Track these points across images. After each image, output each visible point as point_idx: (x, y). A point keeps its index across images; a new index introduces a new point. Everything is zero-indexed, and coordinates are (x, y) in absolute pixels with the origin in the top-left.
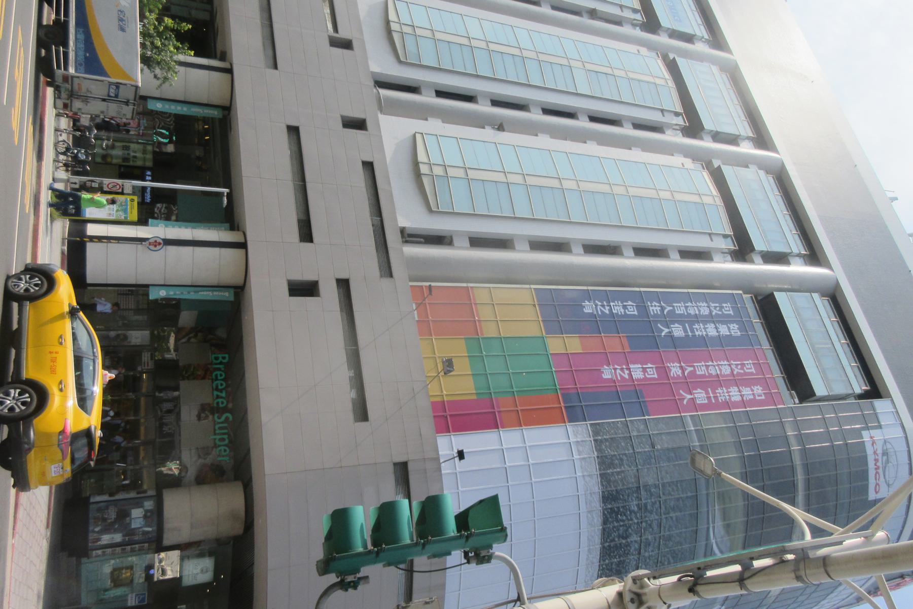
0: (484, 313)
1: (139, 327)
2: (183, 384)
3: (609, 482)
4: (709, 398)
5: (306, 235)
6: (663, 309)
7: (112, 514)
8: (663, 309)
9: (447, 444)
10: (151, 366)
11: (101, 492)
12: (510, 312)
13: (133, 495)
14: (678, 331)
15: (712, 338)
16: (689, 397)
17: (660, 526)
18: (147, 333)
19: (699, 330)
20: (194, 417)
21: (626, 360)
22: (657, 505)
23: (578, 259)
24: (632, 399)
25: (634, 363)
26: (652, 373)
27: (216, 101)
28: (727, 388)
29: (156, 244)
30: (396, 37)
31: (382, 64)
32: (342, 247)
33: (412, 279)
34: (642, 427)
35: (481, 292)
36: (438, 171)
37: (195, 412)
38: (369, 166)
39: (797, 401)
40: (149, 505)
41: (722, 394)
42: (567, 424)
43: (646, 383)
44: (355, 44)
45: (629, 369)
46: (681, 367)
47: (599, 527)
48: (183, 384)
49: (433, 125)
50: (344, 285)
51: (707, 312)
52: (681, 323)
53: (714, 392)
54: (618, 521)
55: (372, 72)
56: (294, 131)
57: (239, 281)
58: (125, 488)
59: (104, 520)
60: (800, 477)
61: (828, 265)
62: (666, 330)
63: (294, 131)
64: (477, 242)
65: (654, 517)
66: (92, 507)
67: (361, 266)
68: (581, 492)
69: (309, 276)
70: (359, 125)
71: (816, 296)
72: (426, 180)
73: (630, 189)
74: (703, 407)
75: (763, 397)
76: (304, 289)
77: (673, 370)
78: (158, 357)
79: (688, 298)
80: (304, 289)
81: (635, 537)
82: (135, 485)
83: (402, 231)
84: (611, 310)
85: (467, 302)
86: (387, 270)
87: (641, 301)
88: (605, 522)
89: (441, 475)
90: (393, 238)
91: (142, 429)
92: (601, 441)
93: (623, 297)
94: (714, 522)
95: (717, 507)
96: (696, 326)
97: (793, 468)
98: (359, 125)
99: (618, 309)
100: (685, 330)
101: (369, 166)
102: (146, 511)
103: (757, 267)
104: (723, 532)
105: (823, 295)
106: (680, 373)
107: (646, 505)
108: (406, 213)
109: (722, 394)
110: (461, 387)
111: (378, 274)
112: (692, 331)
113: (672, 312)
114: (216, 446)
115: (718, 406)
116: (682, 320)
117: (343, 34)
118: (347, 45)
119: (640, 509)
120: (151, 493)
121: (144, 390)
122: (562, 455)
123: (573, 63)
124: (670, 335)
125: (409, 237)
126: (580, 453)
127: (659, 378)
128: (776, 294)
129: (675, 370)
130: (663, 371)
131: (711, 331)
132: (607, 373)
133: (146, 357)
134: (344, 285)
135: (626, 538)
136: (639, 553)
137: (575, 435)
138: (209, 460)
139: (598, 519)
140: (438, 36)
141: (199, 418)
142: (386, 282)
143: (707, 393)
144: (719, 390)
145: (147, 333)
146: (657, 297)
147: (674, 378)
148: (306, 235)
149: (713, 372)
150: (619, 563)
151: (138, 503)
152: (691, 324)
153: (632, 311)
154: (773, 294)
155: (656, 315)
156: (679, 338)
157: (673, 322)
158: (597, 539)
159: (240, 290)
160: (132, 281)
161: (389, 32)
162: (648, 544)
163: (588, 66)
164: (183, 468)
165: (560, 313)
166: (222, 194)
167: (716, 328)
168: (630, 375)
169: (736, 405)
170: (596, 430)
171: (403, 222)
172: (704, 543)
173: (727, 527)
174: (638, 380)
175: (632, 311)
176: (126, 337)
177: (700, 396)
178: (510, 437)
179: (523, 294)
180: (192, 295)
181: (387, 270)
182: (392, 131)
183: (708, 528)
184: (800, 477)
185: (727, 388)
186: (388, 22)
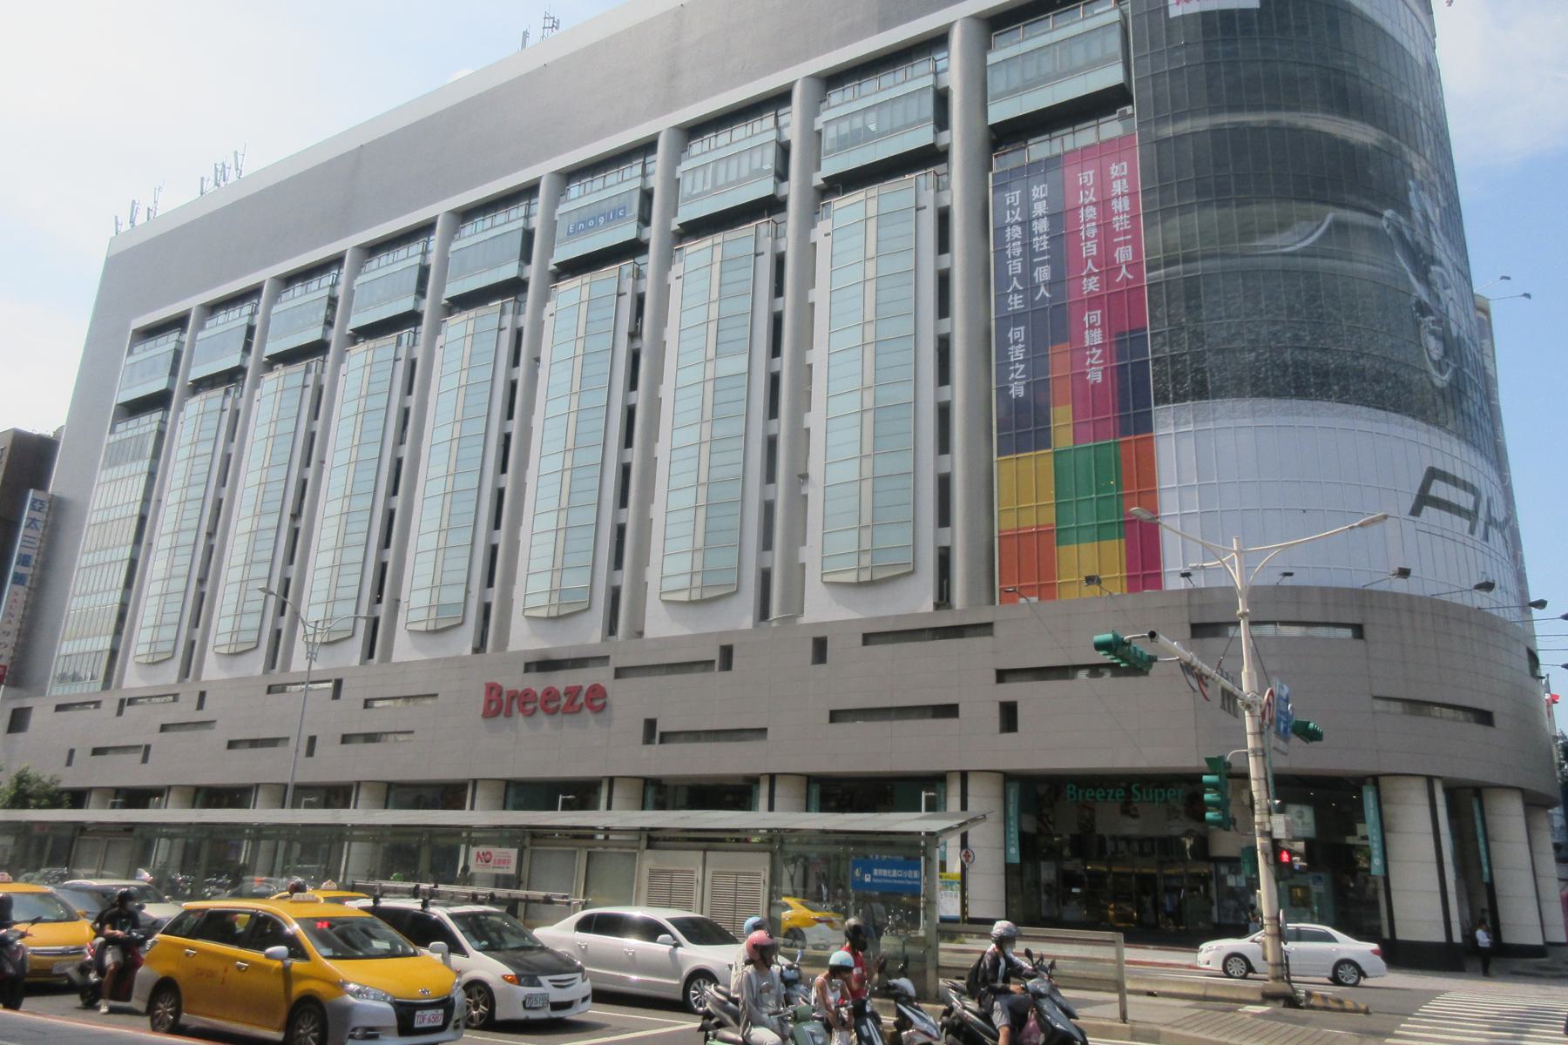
0: (1029, 521)
1: (1037, 871)
2: (1099, 830)
3: (1221, 388)
4: (1126, 243)
5: (950, 711)
6: (1016, 291)
7: (1232, 903)
8: (1016, 291)
9: (1173, 583)
10: (1078, 861)
11: (1209, 913)
12: (1028, 489)
13: (1213, 885)
14: (1043, 274)
15: (1051, 226)
16: (1124, 270)
17: (1275, 323)
18: (1043, 864)
19: (1041, 243)
20: (1135, 822)
21: (1081, 351)
22: (1251, 325)
23: (957, 392)
24: (1125, 341)
25: (1083, 340)
26: (1095, 316)
27: (804, 791)
28: (1113, 215)
29: (967, 856)
30: (707, 595)
31: (740, 616)
32: (960, 673)
33: (993, 603)
34: (1160, 339)
35: (1005, 522)
36: (866, 560)
37: (1130, 820)
38: (868, 639)
39: (1129, 109)
40: (1224, 870)
41: (1120, 222)
42: (1155, 433)
43: (1108, 326)
44: (726, 642)
45: (1091, 347)
46: (1089, 276)
47: (1273, 403)
48: (1099, 830)
49: (810, 555)
50: (1002, 675)
51: (1019, 229)
52: (1033, 267)
53: (1119, 234)
54: (1266, 378)
55: (755, 625)
56: (835, 716)
57: (1000, 776)
58: (1207, 889)
59: (1236, 911)
60: (1225, 119)
61: (950, 26)
62: (1043, 289)
63: (835, 716)
64: (944, 518)
65: (1264, 331)
66: (1224, 921)
67: (979, 656)
68: (1230, 424)
69: (995, 712)
70: (820, 649)
71: (992, 58)
72: (878, 576)
73: (867, 318)
74: (1137, 253)
75: (1125, 164)
76: (1009, 716)
77: (1091, 287)
78: (1066, 852)
79: (1001, 252)
80: (1009, 716)
81: (1287, 356)
82: (1205, 880)
83: (937, 606)
84: (1020, 362)
85: (1017, 538)
86: (986, 628)
87: (1008, 320)
88: (1267, 394)
89: (1206, 589)
90: (946, 619)
91: (1145, 871)
92: (1176, 394)
93: (1004, 345)
94: (1275, 247)
95: (1258, 243)
96: (1036, 246)
97: (1216, 131)
98: (820, 649)
99: (1017, 353)
100: (1042, 263)
101: (868, 639)
102: (1230, 872)
103: (956, 138)
104: (1288, 233)
105: (988, 47)
106: (1095, 279)
107: (1251, 341)
108: (918, 600)
109: (1120, 222)
110: (1111, 556)
111: (988, 639)
112: (1042, 253)
113: (1021, 278)
114: (1166, 801)
115: (1134, 231)
116: (1029, 267)
117: (715, 655)
118: (727, 653)
119: (1253, 350)
120: (1212, 867)
121: (1105, 869)
122: (1188, 444)
123: (709, 375)
124: (1049, 285)
125: (943, 599)
126: (1187, 423)
127: (1102, 308)
128: (991, 121)
129: (1091, 285)
130: (1093, 302)
131: (1041, 226)
132: (1095, 376)
133: (1068, 866)
134: (1002, 675)
135: (1287, 367)
136: (1306, 348)
137: (1168, 425)
138: (1181, 808)
139: (1264, 403)
140: (570, 445)
141: (1135, 817)
142: (997, 629)
143: (1119, 244)
144: (1116, 226)
145: (1043, 864)
146: (1002, 297)
147: (1101, 288)
148: (950, 711)
149: (1094, 232)
150: (1316, 374)
151: (1221, 880)
152: (1032, 251)
153: (1018, 333)
154: (994, 128)
155: (1025, 302)
156: (1053, 273)
157: (1033, 279)
158: (1286, 403)
159: (1008, 777)
160: (1002, 879)
161: (703, 602)
162: (1297, 338)
163: (711, 353)
164: (1188, 834)
165: (1022, 427)
166: (927, 798)
167: (1038, 218)
168: (1097, 346)
169: (1134, 205)
170: (1162, 399)
171: (927, 604)
172: (1300, 260)
173: (1283, 226)
174: (1104, 337)
175: (1018, 333)
176: (1049, 885)
177: (1123, 255)
178: (1169, 506)
179: (1006, 469)
180: (1013, 824)
181: (986, 628)
182: (822, 608)
183: (1284, 254)
184: (1225, 119)
185: (1113, 215)
186: (691, 602)
